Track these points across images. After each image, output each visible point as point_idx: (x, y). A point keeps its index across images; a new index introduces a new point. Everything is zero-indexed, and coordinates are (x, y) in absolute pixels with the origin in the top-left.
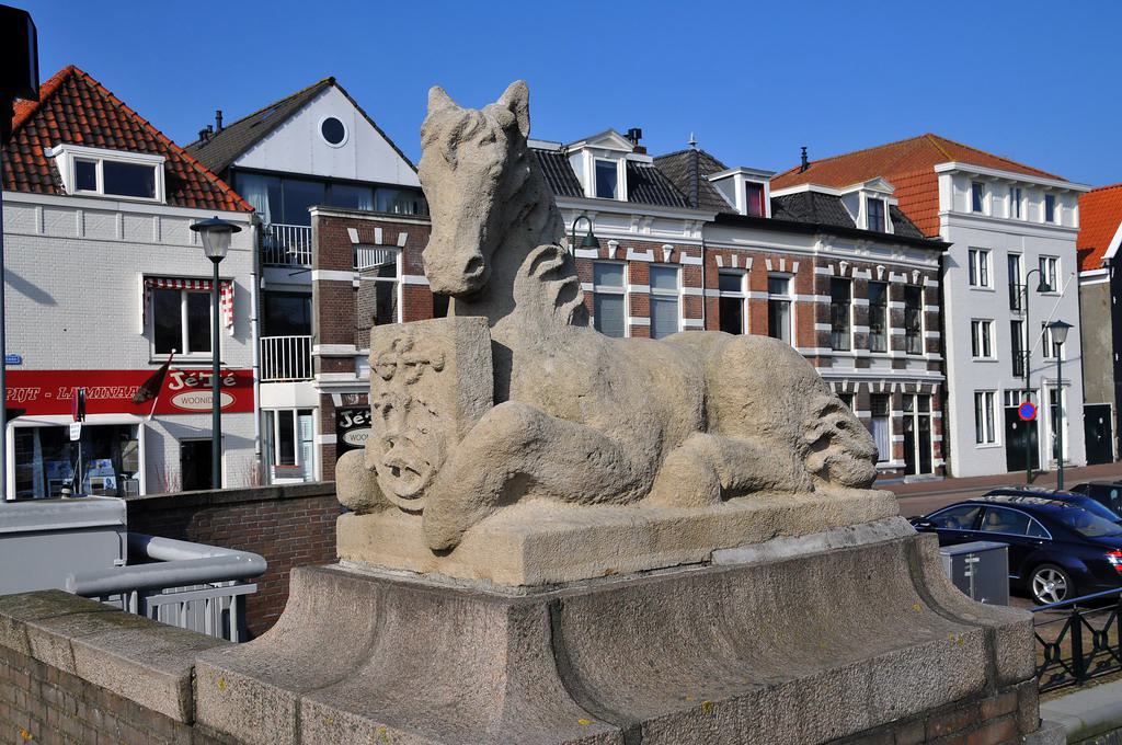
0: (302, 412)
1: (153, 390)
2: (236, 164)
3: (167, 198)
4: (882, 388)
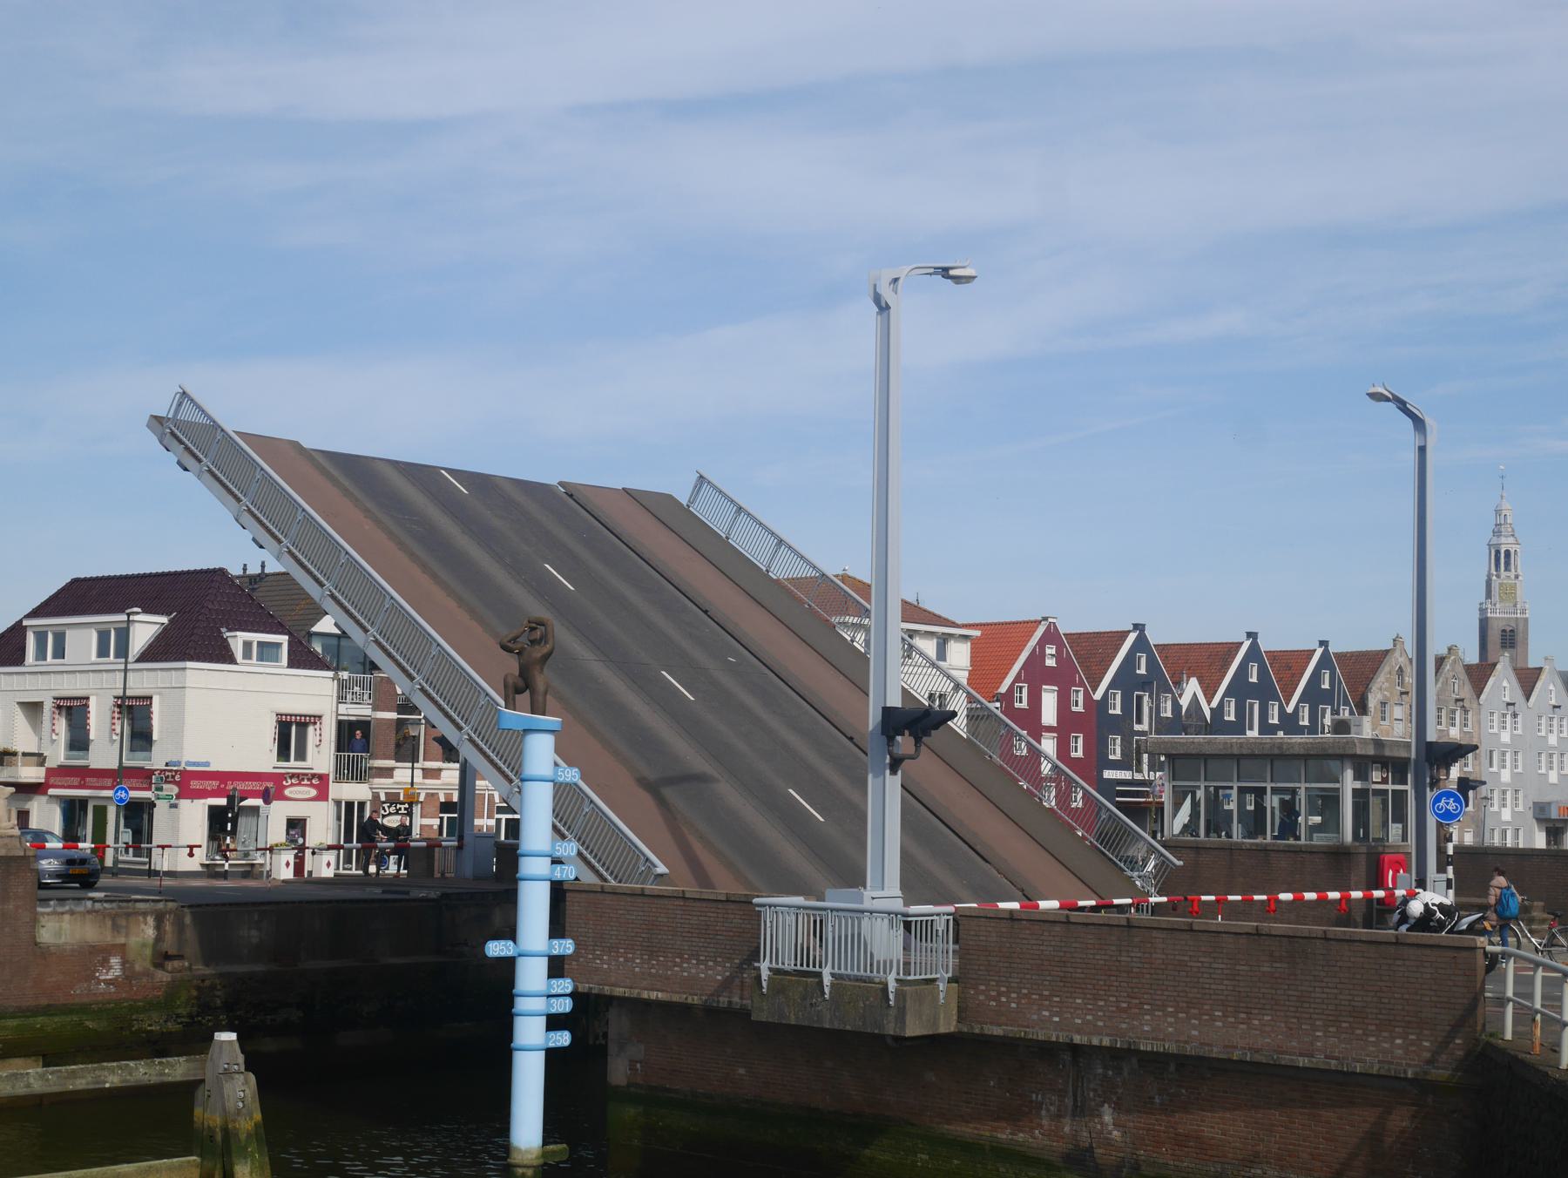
1: (272, 788)
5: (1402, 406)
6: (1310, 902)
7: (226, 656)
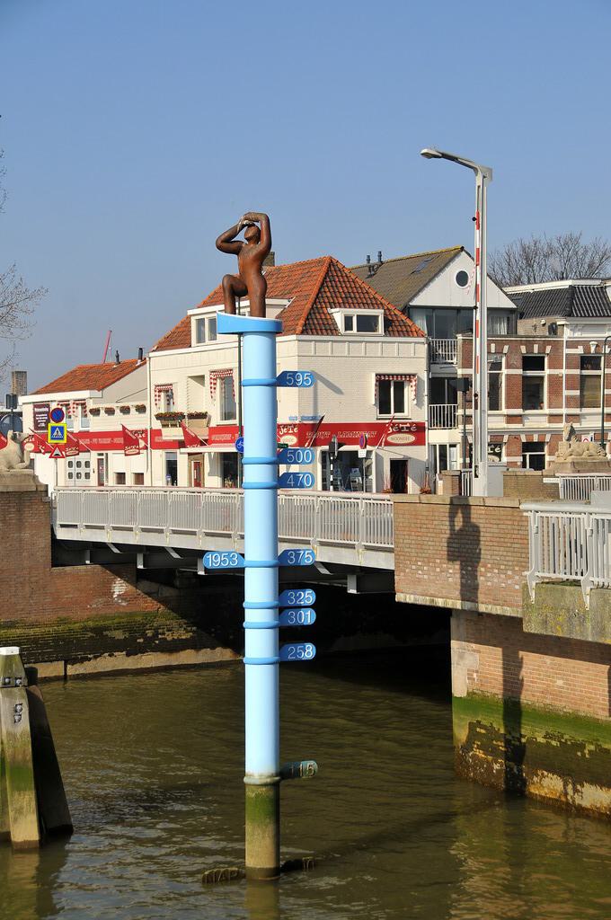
0: (451, 446)
1: (377, 433)
2: (411, 304)
3: (385, 332)
4: (536, 351)
5: (445, 156)
6: (200, 575)
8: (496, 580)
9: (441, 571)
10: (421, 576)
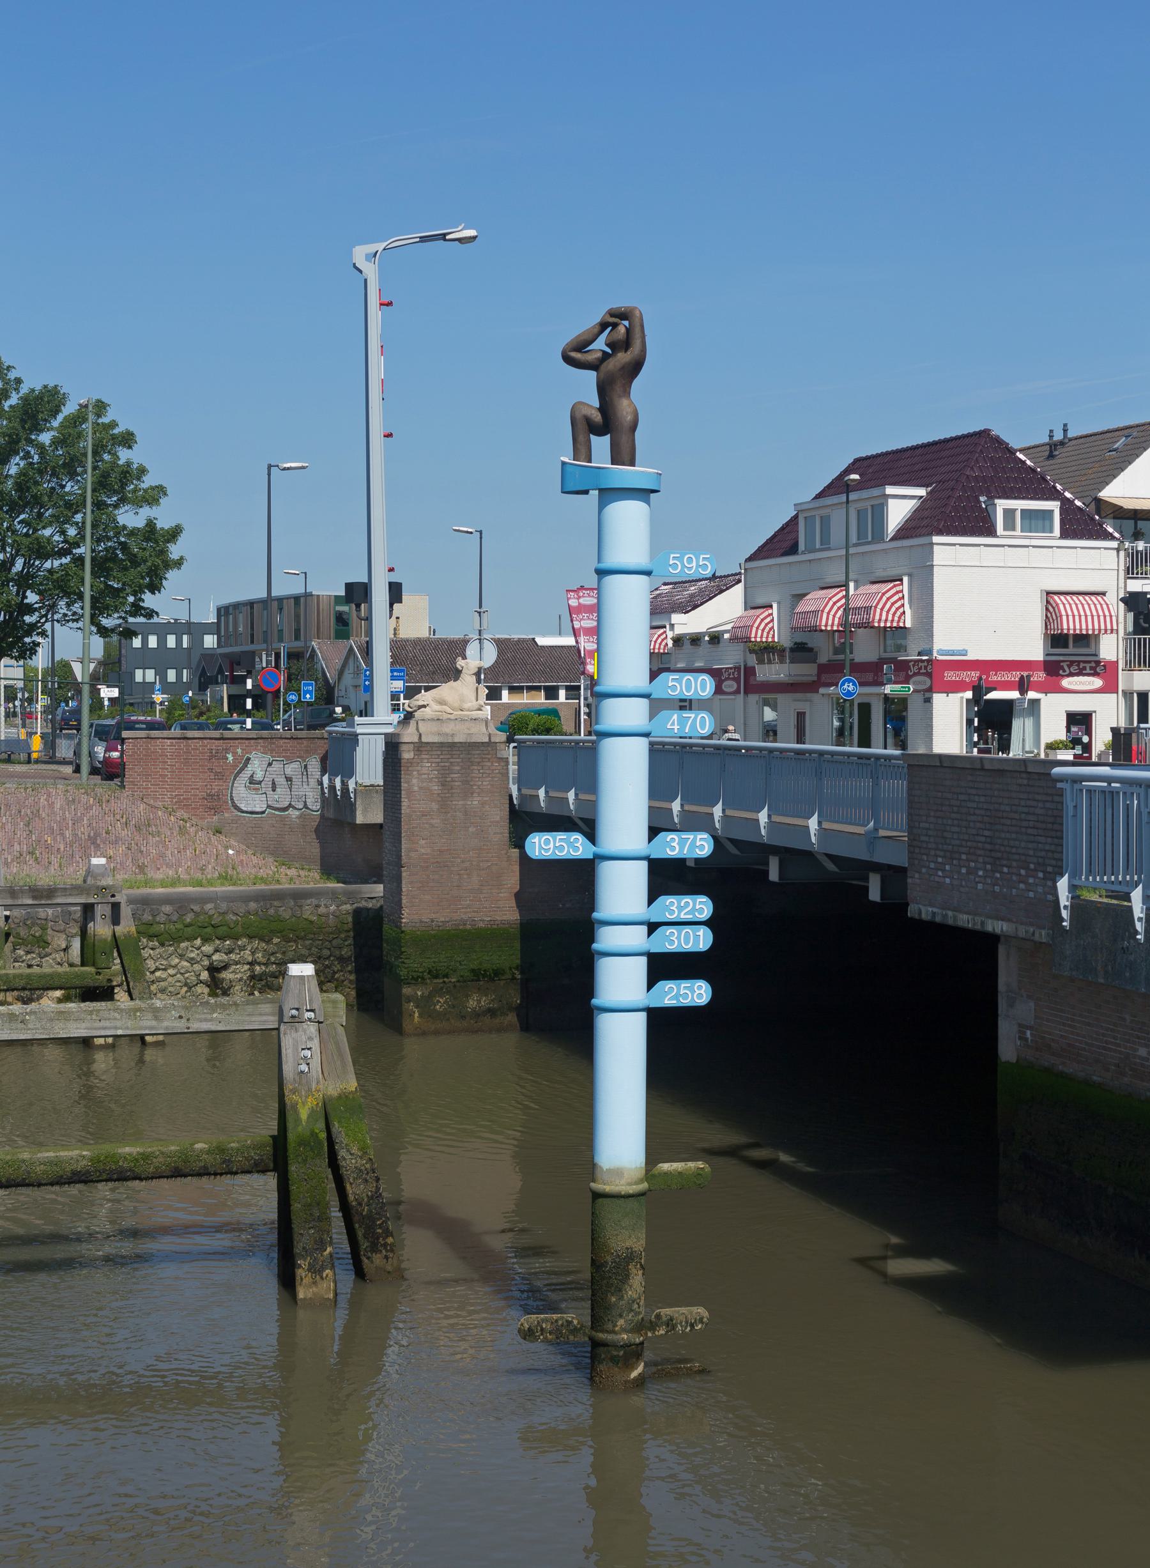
7: (988, 530)
8: (1040, 889)
9: (968, 873)
10: (941, 880)
